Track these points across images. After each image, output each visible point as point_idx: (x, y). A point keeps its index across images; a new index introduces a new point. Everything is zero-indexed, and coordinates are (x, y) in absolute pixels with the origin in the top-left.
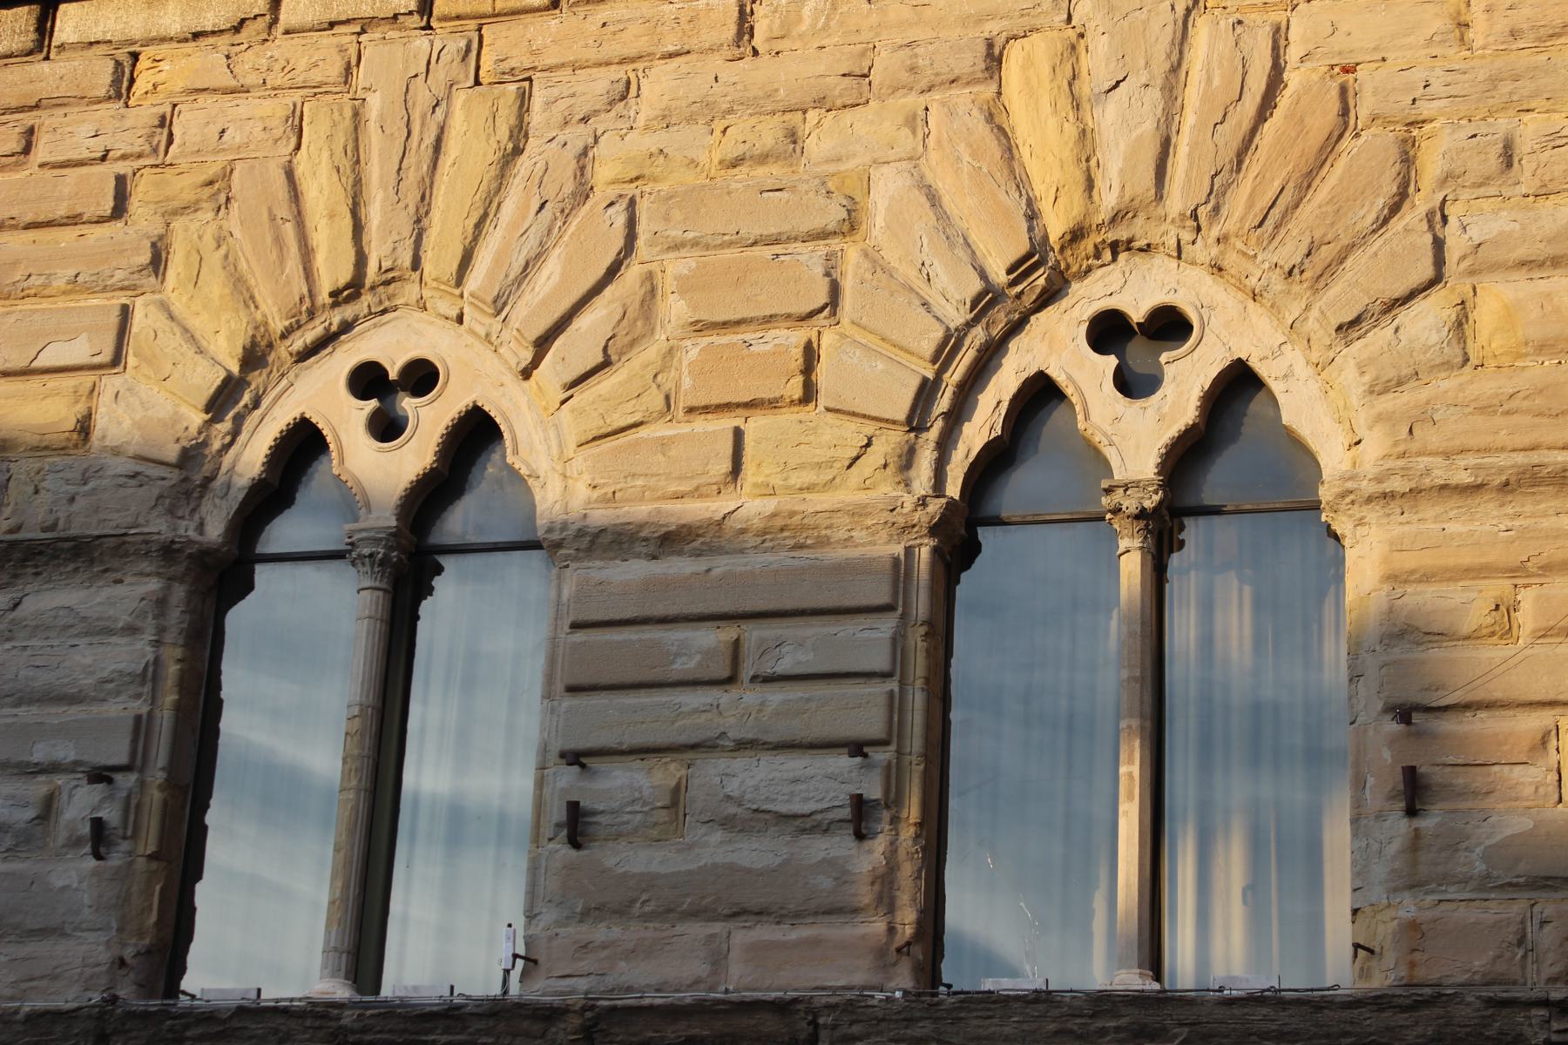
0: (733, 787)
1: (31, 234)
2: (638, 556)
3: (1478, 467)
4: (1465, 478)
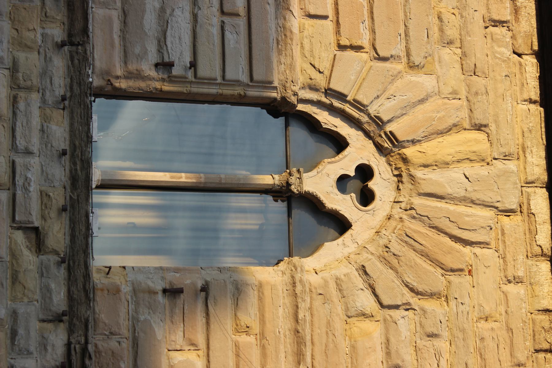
0: (178, 12)
3: (305, 321)
4: (301, 316)
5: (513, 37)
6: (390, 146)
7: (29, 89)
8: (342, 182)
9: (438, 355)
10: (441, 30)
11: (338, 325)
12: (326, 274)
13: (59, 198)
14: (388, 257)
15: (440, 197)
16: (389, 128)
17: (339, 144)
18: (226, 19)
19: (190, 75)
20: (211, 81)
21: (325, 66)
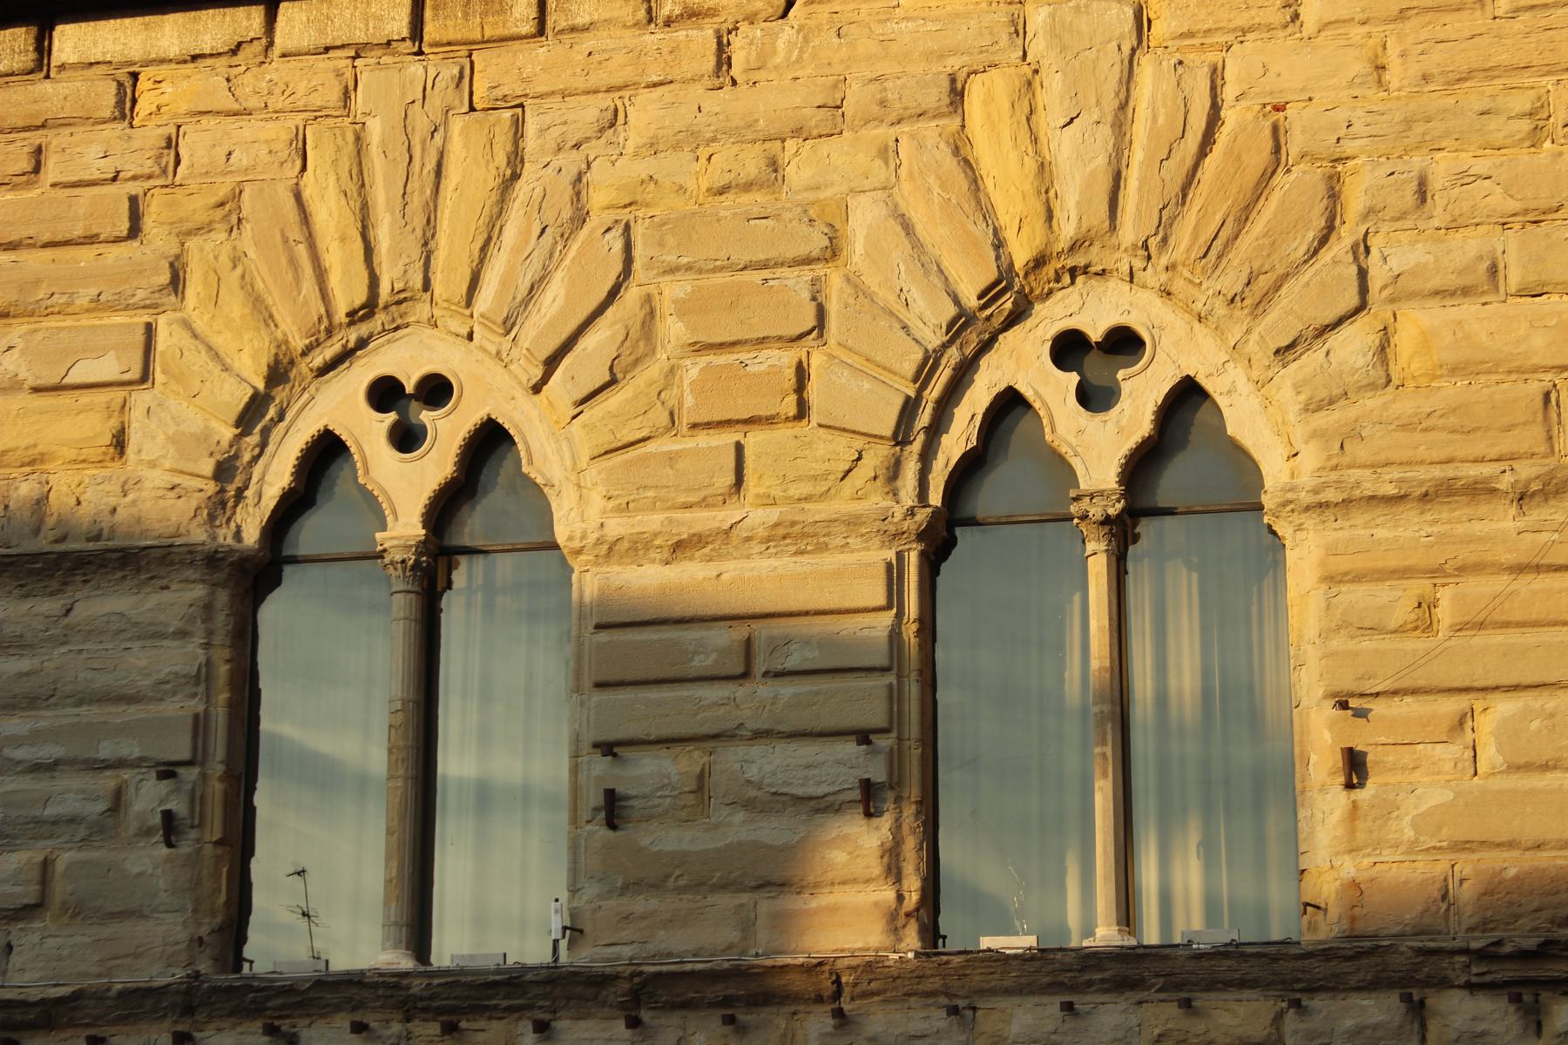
0: (752, 773)
1: (49, 253)
2: (653, 561)
4: (1391, 490)
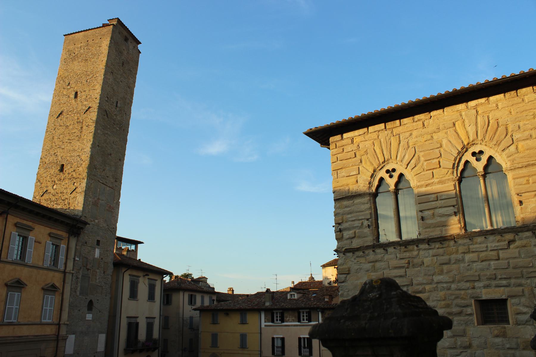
0: (440, 212)
5: (426, 119)
6: (465, 149)
7: (469, 248)
8: (478, 160)
9: (525, 125)
10: (429, 140)
11: (521, 155)
12: (507, 161)
13: (498, 237)
14: (498, 144)
15: (477, 132)
16: (460, 150)
17: (467, 162)
18: (439, 199)
19: (456, 207)
20: (457, 201)
21: (446, 170)
